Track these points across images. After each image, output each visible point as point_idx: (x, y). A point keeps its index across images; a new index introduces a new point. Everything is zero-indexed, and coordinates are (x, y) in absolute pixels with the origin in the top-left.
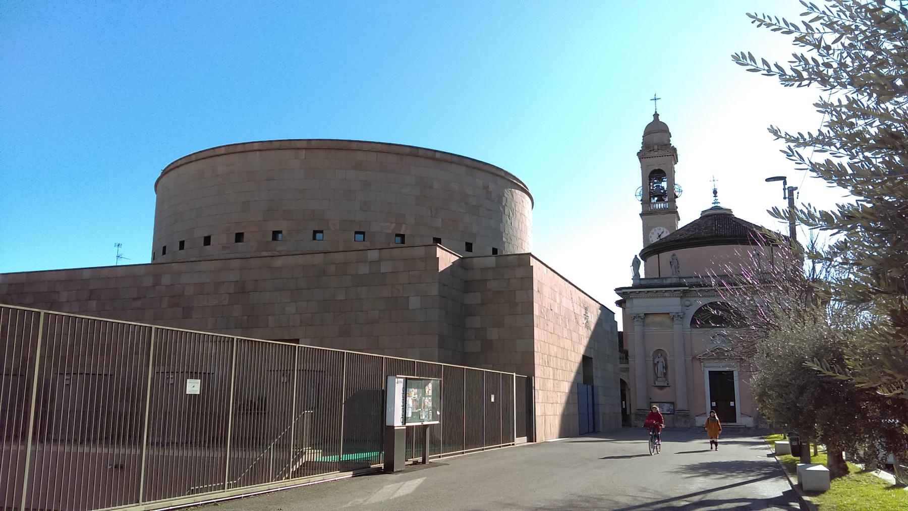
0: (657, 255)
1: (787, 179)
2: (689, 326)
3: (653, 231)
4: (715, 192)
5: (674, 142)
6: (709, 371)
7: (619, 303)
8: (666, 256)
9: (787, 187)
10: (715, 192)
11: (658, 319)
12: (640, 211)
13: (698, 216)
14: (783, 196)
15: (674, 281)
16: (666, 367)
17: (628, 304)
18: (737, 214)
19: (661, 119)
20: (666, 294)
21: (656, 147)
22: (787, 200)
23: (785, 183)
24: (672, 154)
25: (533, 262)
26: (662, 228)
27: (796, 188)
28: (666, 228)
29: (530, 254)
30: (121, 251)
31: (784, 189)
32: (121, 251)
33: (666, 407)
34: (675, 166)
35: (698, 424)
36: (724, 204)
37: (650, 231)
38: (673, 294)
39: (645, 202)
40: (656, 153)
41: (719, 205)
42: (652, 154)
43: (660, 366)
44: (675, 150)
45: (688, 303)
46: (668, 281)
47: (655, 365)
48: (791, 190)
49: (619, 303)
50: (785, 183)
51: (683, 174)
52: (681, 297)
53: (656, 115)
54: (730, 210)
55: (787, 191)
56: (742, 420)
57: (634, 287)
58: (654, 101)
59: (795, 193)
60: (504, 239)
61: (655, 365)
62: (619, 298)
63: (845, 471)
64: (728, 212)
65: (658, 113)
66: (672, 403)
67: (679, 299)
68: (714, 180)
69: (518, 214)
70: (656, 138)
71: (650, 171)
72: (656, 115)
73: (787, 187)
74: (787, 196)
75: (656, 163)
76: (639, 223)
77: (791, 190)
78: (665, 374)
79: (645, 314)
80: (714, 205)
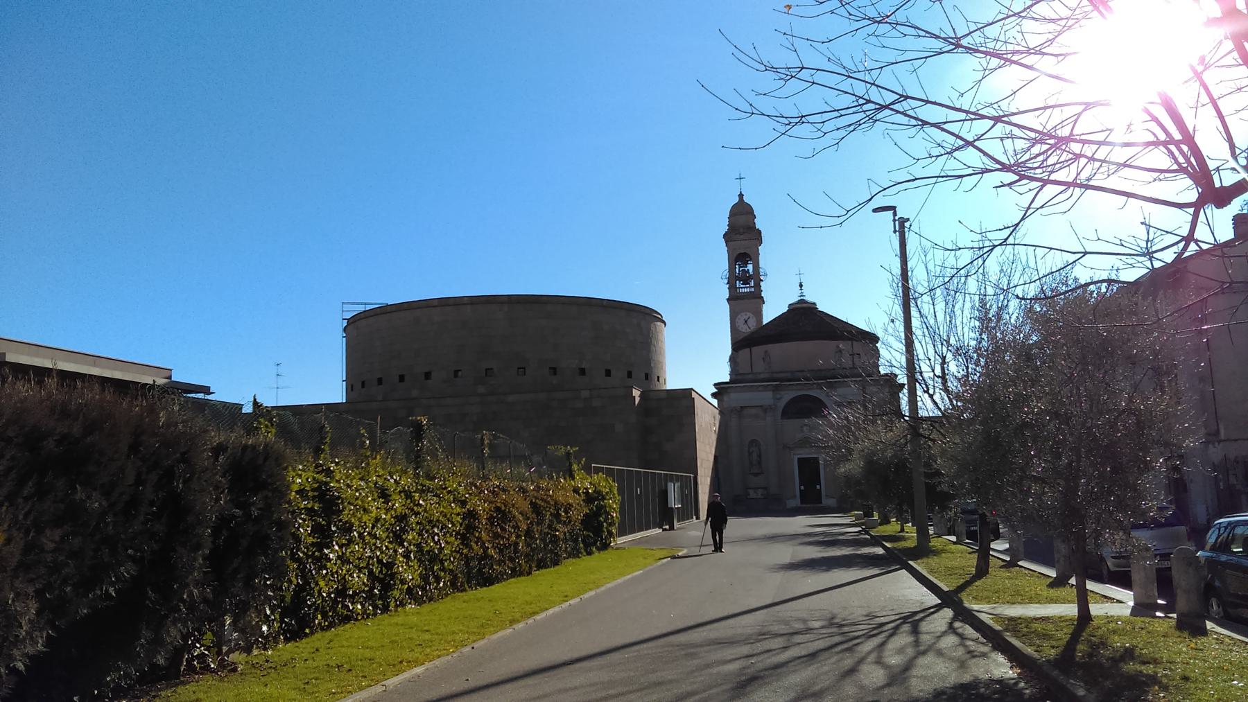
0: (749, 349)
1: (897, 209)
2: (780, 418)
3: (739, 316)
4: (801, 286)
5: (759, 224)
6: (799, 459)
7: (714, 395)
8: (758, 351)
9: (897, 218)
10: (801, 286)
11: (753, 411)
12: (727, 296)
13: (786, 309)
14: (893, 229)
15: (767, 376)
16: (760, 456)
17: (725, 398)
18: (821, 307)
19: (746, 199)
20: (760, 388)
21: (741, 230)
22: (897, 233)
23: (895, 214)
24: (757, 236)
25: (694, 395)
26: (748, 314)
27: (908, 220)
28: (752, 314)
29: (692, 389)
30: (281, 370)
31: (894, 220)
32: (281, 370)
33: (760, 492)
34: (760, 248)
35: (788, 507)
36: (809, 298)
37: (736, 316)
38: (766, 388)
39: (732, 287)
40: (742, 236)
41: (804, 298)
42: (738, 237)
43: (755, 456)
44: (759, 232)
45: (779, 396)
46: (762, 376)
47: (750, 454)
48: (903, 221)
49: (714, 395)
50: (895, 214)
51: (768, 256)
52: (773, 391)
53: (741, 196)
54: (814, 304)
55: (897, 222)
56: (827, 502)
57: (731, 381)
58: (739, 180)
59: (907, 225)
60: (652, 365)
61: (750, 454)
62: (715, 390)
63: (889, 522)
64: (813, 306)
65: (743, 193)
66: (765, 488)
67: (771, 393)
68: (800, 274)
69: (660, 342)
70: (742, 220)
71: (735, 255)
72: (741, 196)
73: (897, 218)
74: (897, 229)
75: (742, 247)
76: (726, 308)
77: (903, 221)
78: (759, 463)
79: (742, 407)
80: (800, 298)
